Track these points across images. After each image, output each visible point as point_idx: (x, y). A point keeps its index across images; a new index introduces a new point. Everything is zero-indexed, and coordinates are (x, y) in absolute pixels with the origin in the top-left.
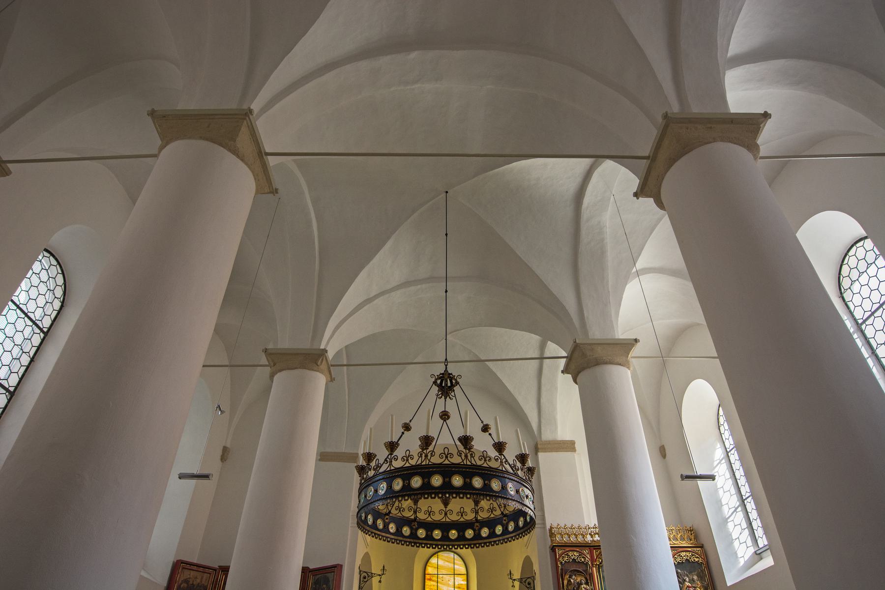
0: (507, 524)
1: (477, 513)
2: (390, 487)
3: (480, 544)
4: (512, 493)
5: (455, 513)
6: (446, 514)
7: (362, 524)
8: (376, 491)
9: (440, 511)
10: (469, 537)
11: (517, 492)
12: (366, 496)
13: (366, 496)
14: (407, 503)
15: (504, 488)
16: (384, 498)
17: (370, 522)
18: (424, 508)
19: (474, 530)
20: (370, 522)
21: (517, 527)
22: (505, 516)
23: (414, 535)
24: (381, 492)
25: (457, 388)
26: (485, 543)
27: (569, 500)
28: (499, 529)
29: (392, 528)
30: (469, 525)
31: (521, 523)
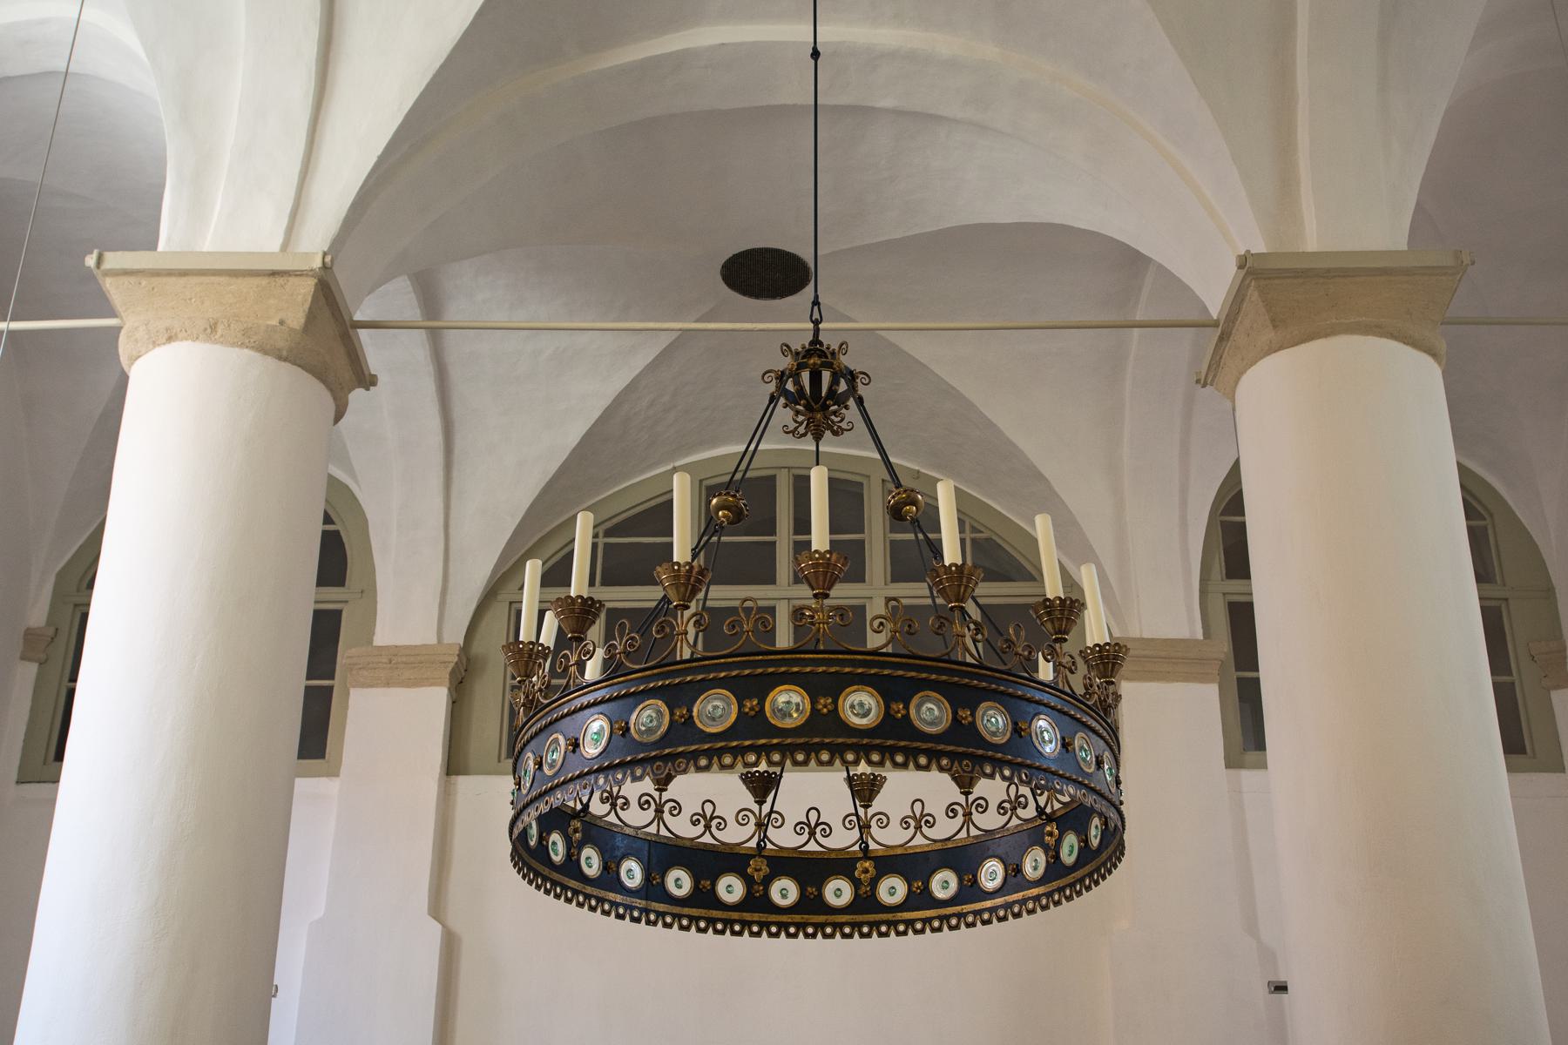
0: (1059, 842)
1: (864, 827)
2: (621, 730)
3: (877, 924)
4: (1048, 749)
5: (790, 825)
6: (967, 815)
7: (530, 859)
8: (575, 745)
9: (741, 815)
10: (990, 885)
11: (1066, 745)
12: (540, 764)
13: (540, 764)
14: (635, 788)
15: (1019, 731)
16: (605, 767)
17: (558, 853)
18: (691, 807)
19: (856, 883)
20: (558, 853)
21: (1055, 868)
22: (1050, 819)
23: (704, 898)
24: (591, 750)
25: (852, 413)
26: (944, 919)
27: (491, 799)
28: (991, 874)
29: (632, 873)
30: (839, 864)
31: (1068, 854)
